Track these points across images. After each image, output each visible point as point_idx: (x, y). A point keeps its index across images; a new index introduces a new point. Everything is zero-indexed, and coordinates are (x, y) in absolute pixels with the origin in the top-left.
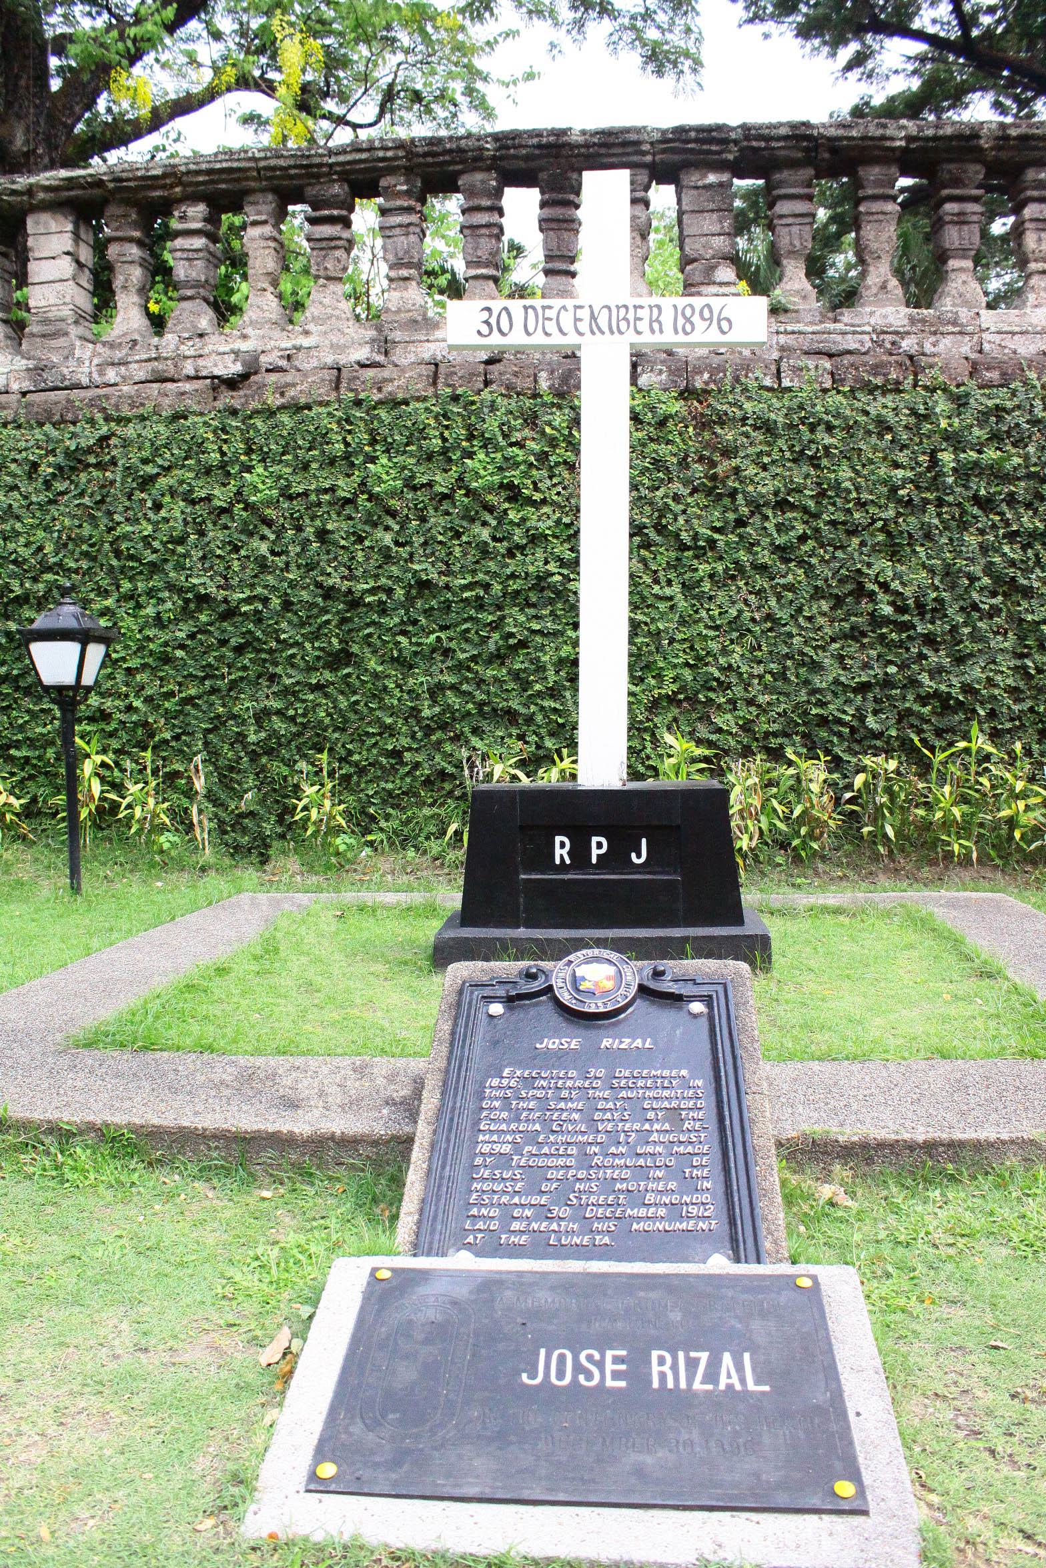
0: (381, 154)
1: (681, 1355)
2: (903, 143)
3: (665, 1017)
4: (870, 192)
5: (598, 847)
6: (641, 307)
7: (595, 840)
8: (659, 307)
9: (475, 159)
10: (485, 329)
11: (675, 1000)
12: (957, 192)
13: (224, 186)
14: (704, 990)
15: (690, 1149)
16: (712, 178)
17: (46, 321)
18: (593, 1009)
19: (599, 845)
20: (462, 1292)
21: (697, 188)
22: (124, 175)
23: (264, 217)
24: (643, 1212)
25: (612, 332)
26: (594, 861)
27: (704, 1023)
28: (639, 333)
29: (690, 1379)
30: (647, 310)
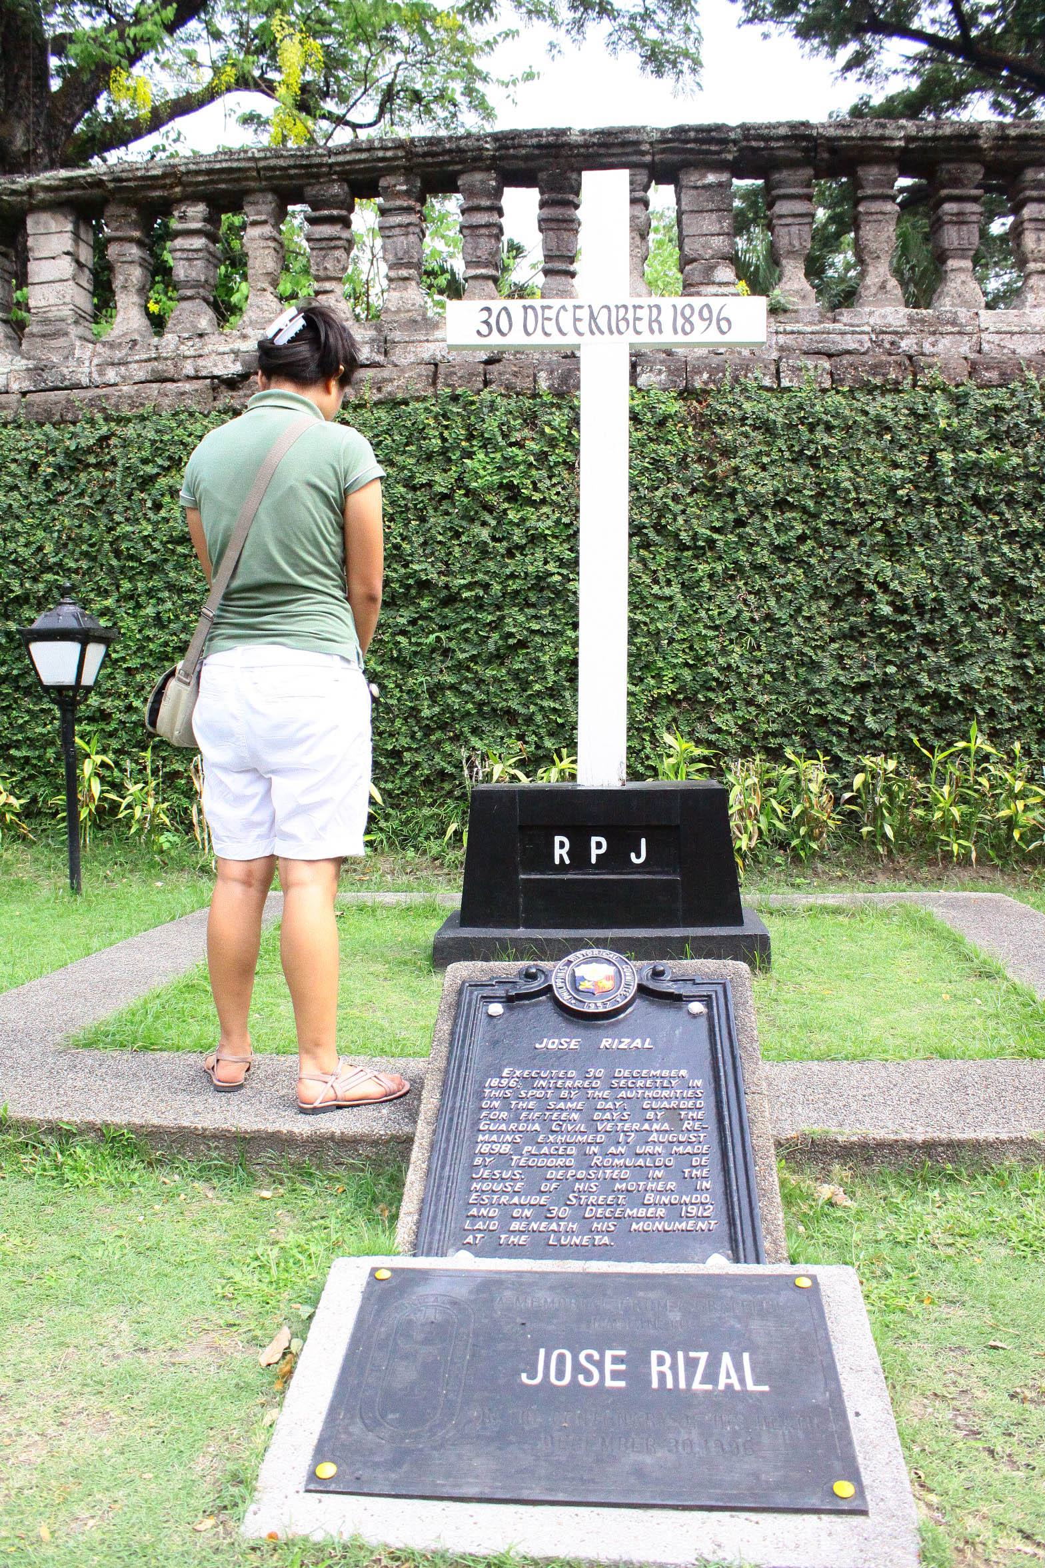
0: (380, 154)
1: (680, 1354)
2: (902, 143)
3: (664, 1017)
4: (869, 192)
5: (598, 847)
6: (641, 307)
7: (594, 840)
8: (658, 307)
9: (475, 159)
10: (484, 329)
11: (675, 1000)
12: (956, 192)
13: (223, 186)
14: (703, 990)
15: (689, 1149)
16: (711, 178)
17: (46, 321)
18: (592, 1009)
19: (599, 845)
20: (462, 1292)
21: (696, 188)
22: (124, 175)
23: (263, 218)
24: (642, 1212)
25: (611, 332)
26: (593, 861)
27: (703, 1023)
28: (638, 333)
29: (690, 1379)
30: (646, 310)
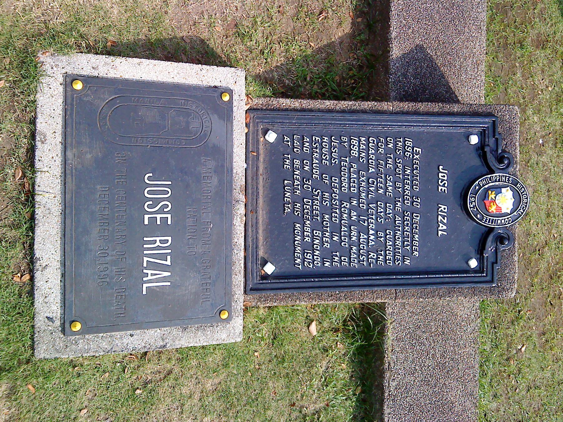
29: (148, 256)
